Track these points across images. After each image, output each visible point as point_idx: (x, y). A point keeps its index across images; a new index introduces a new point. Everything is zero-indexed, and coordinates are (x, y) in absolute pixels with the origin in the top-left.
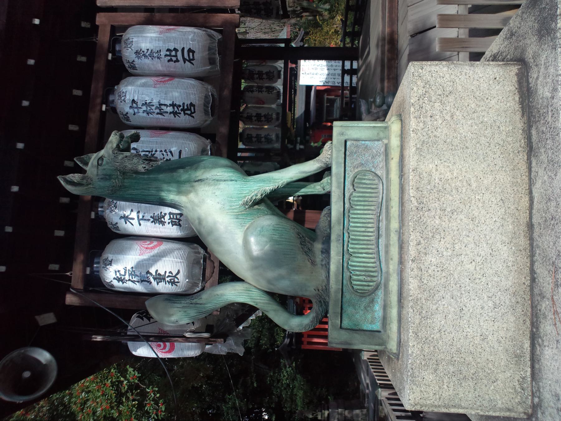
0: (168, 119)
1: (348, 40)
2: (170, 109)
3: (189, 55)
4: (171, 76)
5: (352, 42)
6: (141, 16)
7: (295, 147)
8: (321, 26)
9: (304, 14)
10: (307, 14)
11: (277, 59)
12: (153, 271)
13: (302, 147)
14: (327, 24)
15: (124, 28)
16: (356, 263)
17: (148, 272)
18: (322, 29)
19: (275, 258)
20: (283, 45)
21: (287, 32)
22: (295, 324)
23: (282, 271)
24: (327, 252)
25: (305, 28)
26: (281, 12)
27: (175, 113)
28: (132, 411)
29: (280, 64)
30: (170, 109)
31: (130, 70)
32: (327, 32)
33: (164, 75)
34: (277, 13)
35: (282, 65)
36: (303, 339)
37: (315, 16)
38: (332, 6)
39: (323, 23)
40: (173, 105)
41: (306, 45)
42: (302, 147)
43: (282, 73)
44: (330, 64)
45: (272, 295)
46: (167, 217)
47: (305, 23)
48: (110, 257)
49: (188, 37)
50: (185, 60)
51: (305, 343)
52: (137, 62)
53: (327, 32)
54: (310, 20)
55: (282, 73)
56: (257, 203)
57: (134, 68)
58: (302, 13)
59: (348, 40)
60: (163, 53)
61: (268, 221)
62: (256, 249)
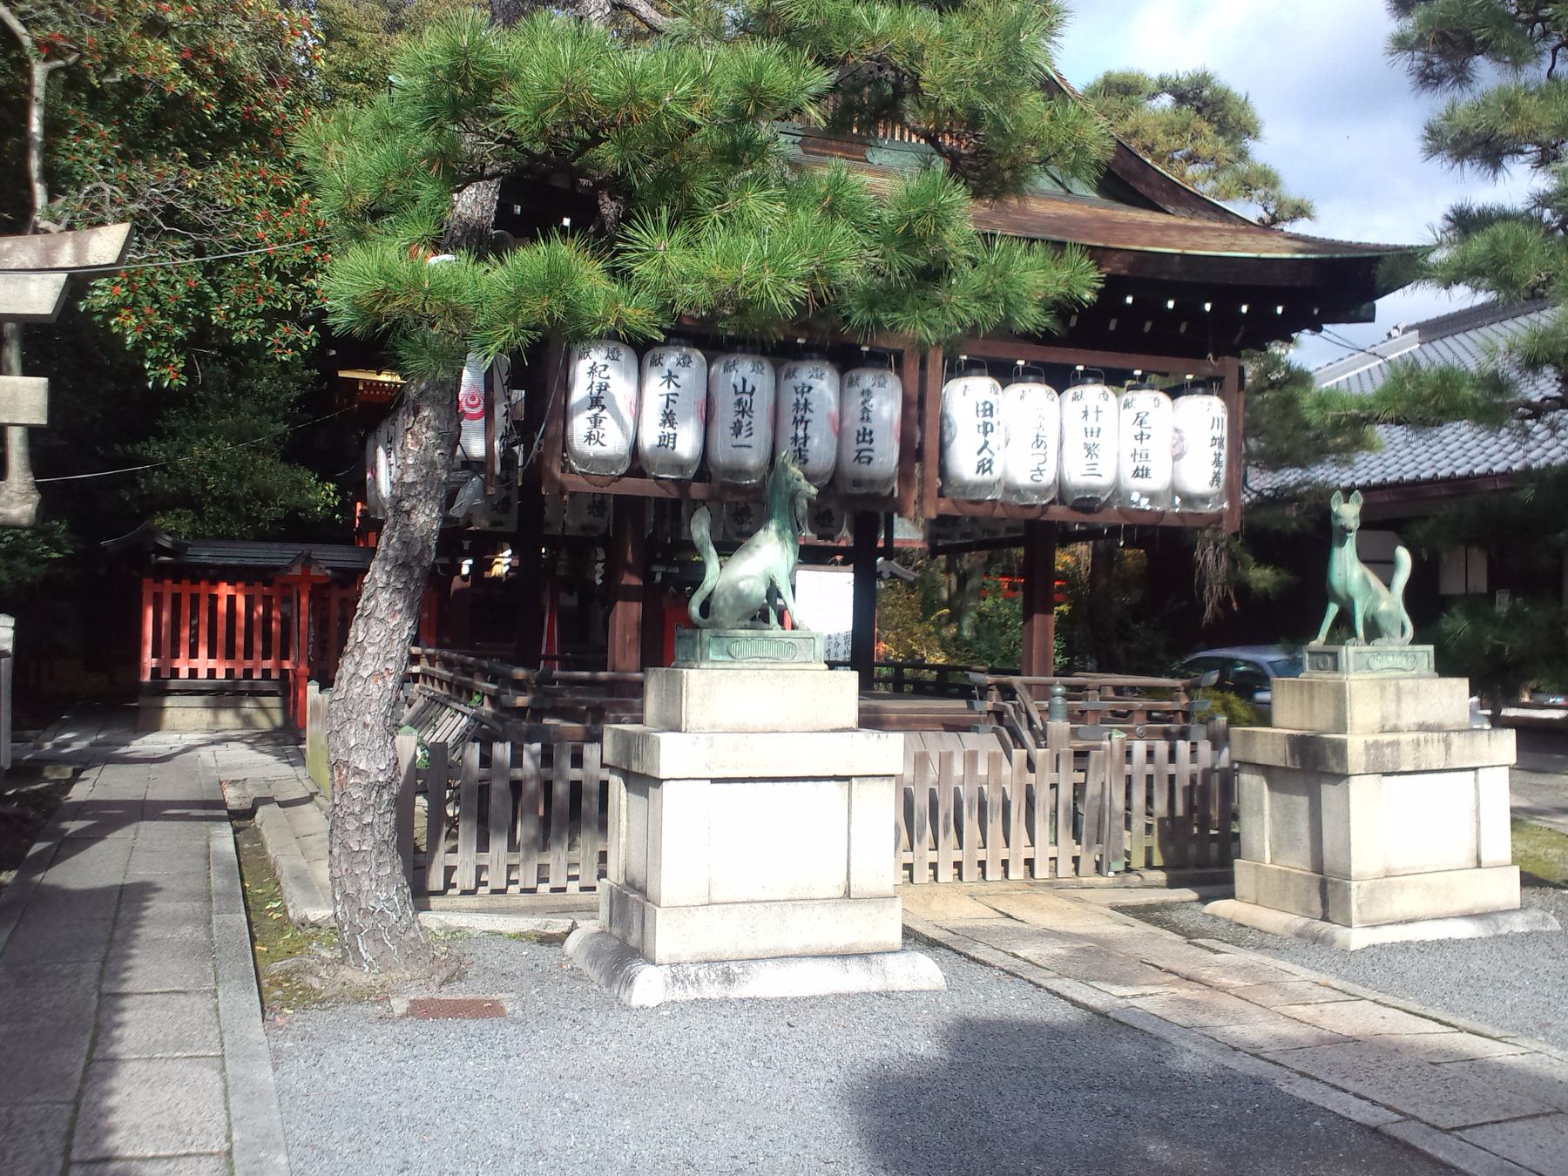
0: (788, 430)
1: (885, 671)
2: (801, 434)
3: (864, 458)
4: (840, 433)
5: (886, 680)
6: (914, 390)
7: (658, 562)
8: (925, 618)
9: (954, 579)
10: (954, 587)
11: (857, 531)
12: (604, 413)
13: (658, 578)
14: (930, 634)
15: (900, 373)
16: (743, 644)
17: (604, 407)
18: (920, 622)
19: (740, 597)
20: (881, 544)
21: (911, 541)
22: (695, 609)
23: (731, 601)
24: (746, 628)
25: (920, 581)
26: (940, 543)
27: (796, 439)
28: (276, 300)
29: (845, 538)
30: (801, 434)
31: (847, 375)
32: (911, 634)
33: (841, 421)
34: (939, 536)
35: (843, 544)
36: (168, 583)
37: (948, 604)
38: (968, 643)
39: (933, 623)
40: (806, 438)
41: (881, 585)
42: (658, 578)
43: (829, 543)
44: (842, 642)
45: (710, 594)
46: (671, 431)
47: (933, 580)
48: (622, 358)
49: (886, 455)
50: (860, 451)
51: (158, 588)
52: (857, 390)
53: (911, 634)
54: (938, 592)
55: (829, 543)
56: (772, 583)
57: (851, 384)
58: (957, 574)
59: (885, 671)
60: (869, 426)
61: (762, 590)
62: (742, 585)
